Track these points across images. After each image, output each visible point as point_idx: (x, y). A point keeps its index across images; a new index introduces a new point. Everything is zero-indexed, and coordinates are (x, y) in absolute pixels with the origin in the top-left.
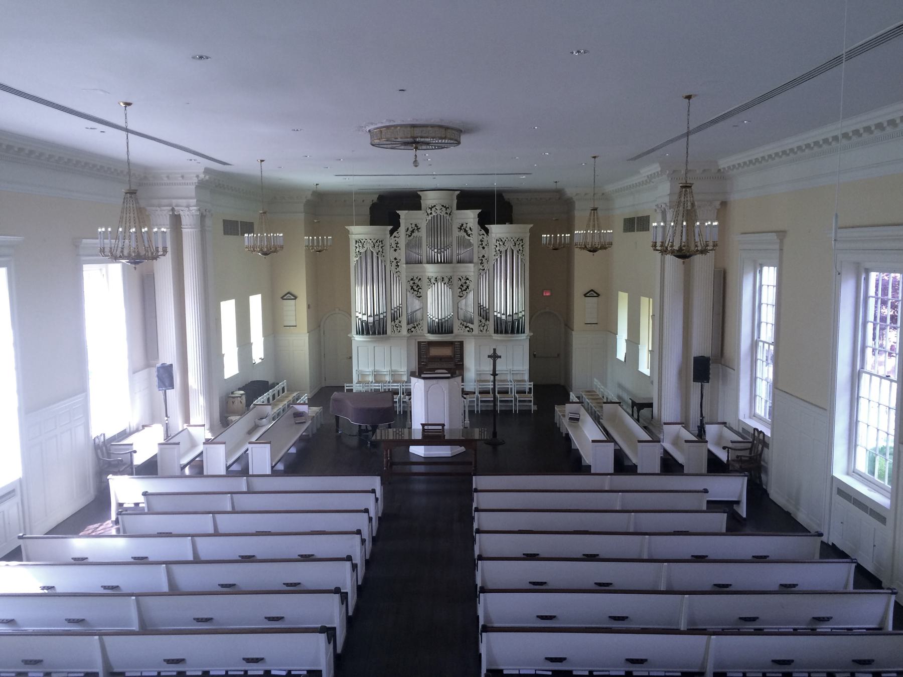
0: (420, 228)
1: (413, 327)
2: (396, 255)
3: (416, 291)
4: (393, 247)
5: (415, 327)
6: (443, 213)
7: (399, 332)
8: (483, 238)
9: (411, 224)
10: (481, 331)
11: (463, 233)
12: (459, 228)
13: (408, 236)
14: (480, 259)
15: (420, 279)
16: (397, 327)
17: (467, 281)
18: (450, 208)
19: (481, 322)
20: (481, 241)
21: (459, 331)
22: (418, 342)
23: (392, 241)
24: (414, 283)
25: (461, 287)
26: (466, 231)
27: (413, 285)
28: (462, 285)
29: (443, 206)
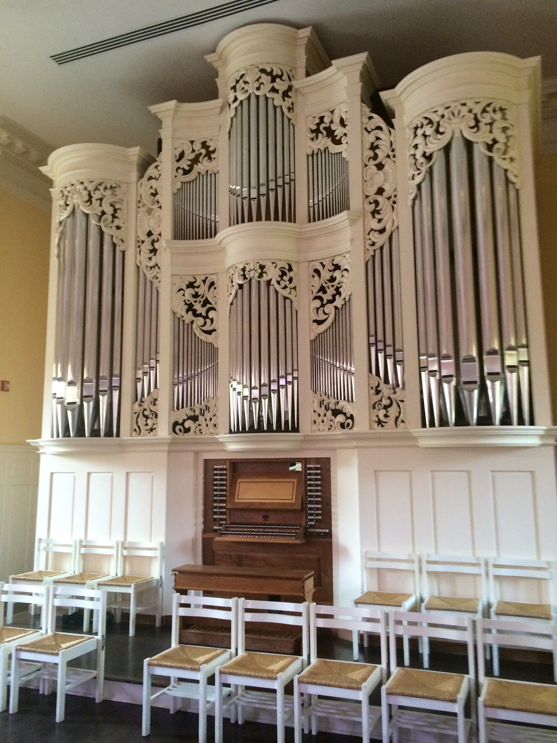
0: (214, 152)
1: (190, 418)
2: (150, 224)
3: (200, 315)
4: (144, 205)
5: (194, 419)
6: (265, 90)
7: (152, 430)
8: (378, 138)
9: (192, 142)
10: (379, 422)
11: (323, 142)
12: (312, 131)
13: (181, 171)
14: (371, 199)
15: (212, 284)
16: (147, 417)
17: (337, 274)
18: (285, 77)
19: (378, 392)
20: (373, 147)
21: (315, 427)
22: (206, 461)
23: (142, 190)
24: (196, 295)
25: (321, 294)
26: (330, 133)
27: (192, 300)
28: (323, 289)
29: (263, 71)
